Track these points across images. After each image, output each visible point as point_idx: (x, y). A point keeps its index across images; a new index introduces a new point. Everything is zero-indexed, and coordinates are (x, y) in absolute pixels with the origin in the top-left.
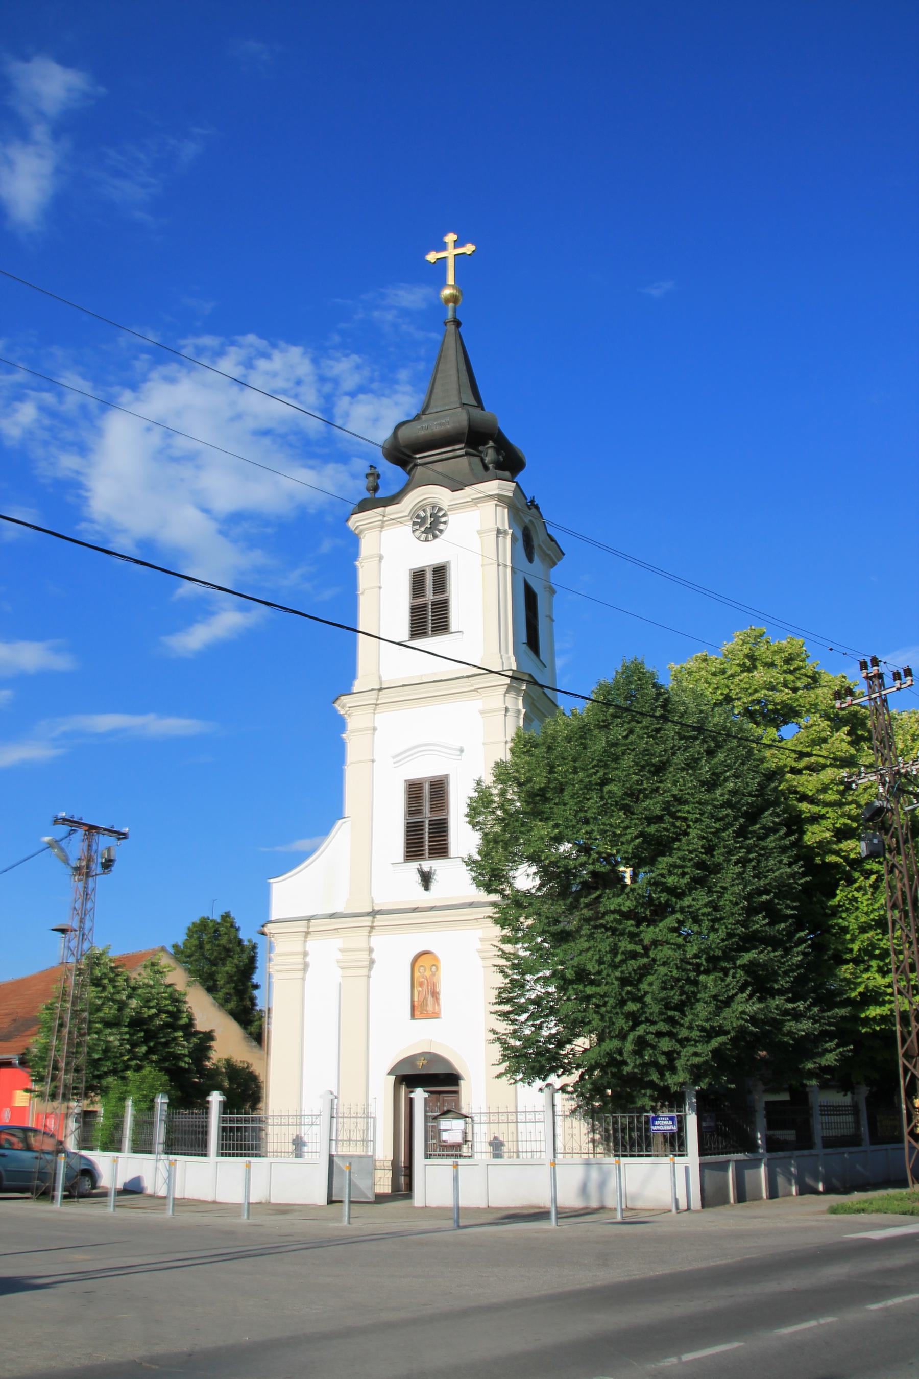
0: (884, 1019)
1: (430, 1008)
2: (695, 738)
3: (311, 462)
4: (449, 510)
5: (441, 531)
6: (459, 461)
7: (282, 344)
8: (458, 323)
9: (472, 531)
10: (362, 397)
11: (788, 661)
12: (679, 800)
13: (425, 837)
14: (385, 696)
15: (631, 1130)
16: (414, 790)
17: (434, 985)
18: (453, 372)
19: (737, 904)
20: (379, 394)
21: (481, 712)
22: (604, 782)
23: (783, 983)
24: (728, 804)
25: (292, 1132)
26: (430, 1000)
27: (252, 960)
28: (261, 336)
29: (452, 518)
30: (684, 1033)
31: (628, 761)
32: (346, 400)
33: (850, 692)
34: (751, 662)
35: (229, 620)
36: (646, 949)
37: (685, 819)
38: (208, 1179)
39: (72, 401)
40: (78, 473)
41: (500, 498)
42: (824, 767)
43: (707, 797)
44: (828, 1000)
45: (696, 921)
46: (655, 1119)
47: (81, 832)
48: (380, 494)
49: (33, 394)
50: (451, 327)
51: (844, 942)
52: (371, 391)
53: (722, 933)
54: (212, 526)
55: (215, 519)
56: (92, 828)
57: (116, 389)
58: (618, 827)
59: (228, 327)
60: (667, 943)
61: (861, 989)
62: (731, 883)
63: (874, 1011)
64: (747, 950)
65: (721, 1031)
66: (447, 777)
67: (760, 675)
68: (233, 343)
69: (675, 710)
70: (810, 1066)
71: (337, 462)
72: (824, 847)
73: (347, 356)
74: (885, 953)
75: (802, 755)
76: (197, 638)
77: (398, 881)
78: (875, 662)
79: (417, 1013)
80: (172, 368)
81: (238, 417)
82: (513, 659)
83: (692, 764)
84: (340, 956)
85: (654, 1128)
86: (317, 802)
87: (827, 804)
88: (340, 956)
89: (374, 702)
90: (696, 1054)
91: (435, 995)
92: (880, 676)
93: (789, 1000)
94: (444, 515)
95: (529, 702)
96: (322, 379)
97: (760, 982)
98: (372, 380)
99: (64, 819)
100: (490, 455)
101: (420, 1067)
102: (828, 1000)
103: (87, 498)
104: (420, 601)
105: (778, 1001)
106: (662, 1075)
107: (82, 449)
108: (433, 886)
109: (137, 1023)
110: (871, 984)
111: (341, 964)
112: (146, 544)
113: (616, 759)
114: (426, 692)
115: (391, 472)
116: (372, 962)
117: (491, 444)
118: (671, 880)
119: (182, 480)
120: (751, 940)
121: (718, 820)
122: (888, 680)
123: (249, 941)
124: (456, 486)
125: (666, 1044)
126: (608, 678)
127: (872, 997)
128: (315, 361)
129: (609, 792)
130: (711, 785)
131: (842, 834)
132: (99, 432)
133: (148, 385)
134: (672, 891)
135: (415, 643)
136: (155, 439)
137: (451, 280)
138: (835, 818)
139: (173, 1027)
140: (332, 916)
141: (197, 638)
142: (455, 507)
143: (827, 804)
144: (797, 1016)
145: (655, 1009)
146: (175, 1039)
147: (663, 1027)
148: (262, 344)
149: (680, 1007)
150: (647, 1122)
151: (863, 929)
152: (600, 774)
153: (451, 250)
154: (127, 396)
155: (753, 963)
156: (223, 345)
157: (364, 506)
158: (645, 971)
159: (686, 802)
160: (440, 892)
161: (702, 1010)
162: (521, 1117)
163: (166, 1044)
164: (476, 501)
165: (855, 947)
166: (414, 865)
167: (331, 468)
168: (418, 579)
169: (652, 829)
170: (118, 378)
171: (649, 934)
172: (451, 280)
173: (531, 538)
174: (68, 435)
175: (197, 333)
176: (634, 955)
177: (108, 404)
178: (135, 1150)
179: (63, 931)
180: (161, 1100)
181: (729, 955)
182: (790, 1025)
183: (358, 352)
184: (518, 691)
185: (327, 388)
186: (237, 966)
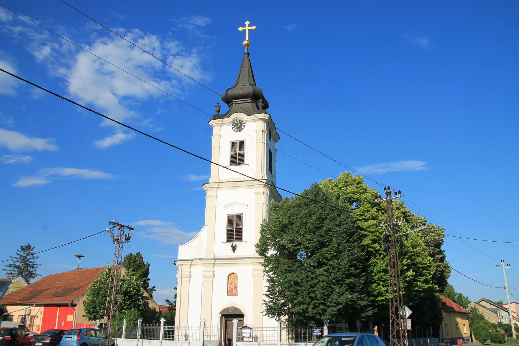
0: (382, 301)
1: (234, 292)
2: (335, 210)
3: (156, 79)
5: (243, 129)
6: (249, 104)
7: (149, 34)
8: (248, 54)
9: (253, 131)
10: (177, 57)
11: (358, 184)
12: (330, 231)
13: (234, 233)
15: (306, 334)
16: (230, 218)
18: (247, 72)
19: (346, 264)
20: (184, 56)
21: (255, 193)
22: (306, 223)
23: (357, 289)
24: (344, 232)
25: (185, 332)
27: (148, 270)
28: (141, 30)
29: (246, 125)
30: (329, 304)
31: (314, 217)
32: (172, 57)
33: (380, 197)
34: (347, 184)
35: (120, 137)
36: (317, 277)
37: (331, 236)
39: (65, 48)
40: (65, 75)
41: (264, 120)
42: (369, 220)
43: (339, 229)
44: (369, 294)
45: (333, 269)
47: (118, 227)
48: (219, 114)
49: (50, 43)
50: (246, 55)
51: (372, 276)
52: (182, 55)
53: (341, 272)
54: (116, 100)
55: (118, 97)
56: (122, 226)
57: (83, 45)
58: (311, 238)
59: (129, 26)
60: (323, 275)
61: (377, 292)
62: (345, 257)
63: (380, 298)
64: (348, 279)
65: (339, 304)
67: (350, 189)
68: (130, 32)
69: (329, 201)
70: (363, 315)
71: (166, 80)
72: (368, 246)
73: (173, 41)
74: (386, 280)
75: (361, 215)
76: (107, 142)
77: (224, 248)
78: (389, 188)
79: (229, 293)
80: (106, 39)
81: (130, 60)
82: (266, 175)
83: (334, 219)
84: (202, 273)
86: (193, 220)
87: (370, 232)
88: (202, 273)
90: (333, 311)
91: (236, 288)
92: (390, 193)
93: (359, 294)
94: (244, 123)
95: (270, 191)
96: (163, 49)
97: (351, 288)
98: (182, 51)
99: (113, 223)
100: (260, 104)
101: (231, 312)
102: (369, 294)
103: (67, 86)
104: (234, 153)
105: (356, 295)
106: (321, 316)
107: (68, 67)
108: (236, 251)
109: (126, 293)
110: (381, 290)
112: (91, 104)
113: (310, 216)
115: (224, 107)
116: (214, 276)
117: (261, 100)
118: (326, 255)
119: (106, 82)
120: (349, 276)
121: (342, 237)
122: (393, 194)
123: (147, 263)
124: (249, 114)
125: (322, 307)
126: (308, 188)
127: (380, 294)
128: (161, 42)
129: (308, 227)
130: (339, 225)
131: (374, 241)
132: (75, 61)
133: (95, 44)
134: (326, 258)
135: (234, 168)
136: (97, 65)
137: (247, 39)
138: (372, 236)
139: (138, 295)
140: (200, 259)
141: (107, 142)
142: (248, 121)
143: (370, 232)
144: (361, 299)
145: (319, 296)
146: (139, 299)
147: (322, 301)
148: (141, 33)
149: (328, 295)
150: (312, 331)
151: (379, 272)
152: (305, 220)
153: (247, 27)
154: (87, 48)
155: (350, 283)
156: (125, 32)
157: (216, 117)
158: (316, 284)
159: (332, 231)
160: (239, 252)
161: (335, 297)
163: (135, 301)
164: (255, 120)
165: (376, 277)
166: (231, 243)
167: (163, 83)
168: (234, 145)
169: (321, 239)
170: (84, 41)
171: (318, 272)
172: (247, 39)
173: (272, 133)
174: (63, 61)
175: (117, 27)
176: (312, 279)
177: (80, 49)
178: (127, 337)
179: (79, 257)
180: (140, 321)
181: (343, 279)
182: (359, 302)
183: (178, 40)
184: (267, 187)
185: (165, 52)
186: (143, 272)
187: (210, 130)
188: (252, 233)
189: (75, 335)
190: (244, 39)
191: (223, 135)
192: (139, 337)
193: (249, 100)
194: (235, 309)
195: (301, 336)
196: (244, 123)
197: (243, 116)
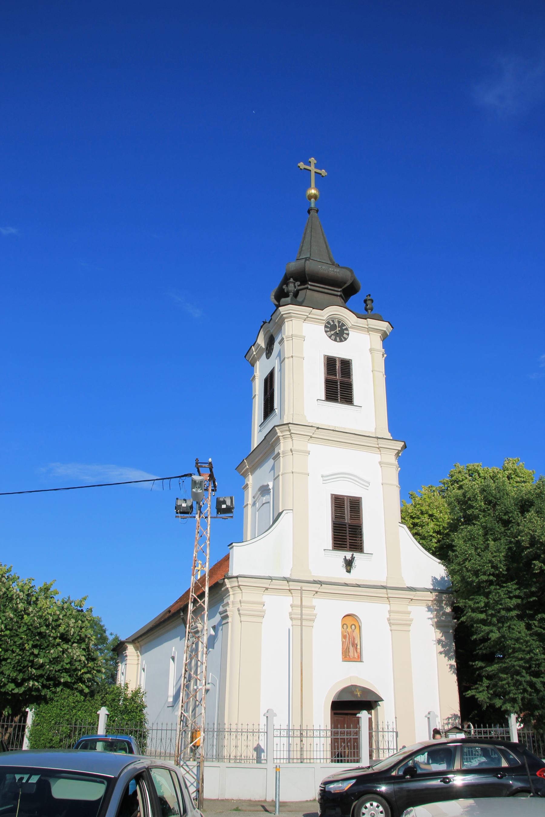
1: (351, 654)
4: (351, 328)
5: (346, 339)
9: (365, 347)
13: (347, 531)
14: (320, 434)
16: (338, 502)
17: (354, 638)
26: (351, 649)
29: (351, 333)
66: (332, 495)
89: (311, 434)
91: (354, 645)
142: (355, 327)
164: (369, 330)
188: (381, 519)
193: (338, 291)
194: (366, 691)
196: (347, 329)
197: (348, 317)
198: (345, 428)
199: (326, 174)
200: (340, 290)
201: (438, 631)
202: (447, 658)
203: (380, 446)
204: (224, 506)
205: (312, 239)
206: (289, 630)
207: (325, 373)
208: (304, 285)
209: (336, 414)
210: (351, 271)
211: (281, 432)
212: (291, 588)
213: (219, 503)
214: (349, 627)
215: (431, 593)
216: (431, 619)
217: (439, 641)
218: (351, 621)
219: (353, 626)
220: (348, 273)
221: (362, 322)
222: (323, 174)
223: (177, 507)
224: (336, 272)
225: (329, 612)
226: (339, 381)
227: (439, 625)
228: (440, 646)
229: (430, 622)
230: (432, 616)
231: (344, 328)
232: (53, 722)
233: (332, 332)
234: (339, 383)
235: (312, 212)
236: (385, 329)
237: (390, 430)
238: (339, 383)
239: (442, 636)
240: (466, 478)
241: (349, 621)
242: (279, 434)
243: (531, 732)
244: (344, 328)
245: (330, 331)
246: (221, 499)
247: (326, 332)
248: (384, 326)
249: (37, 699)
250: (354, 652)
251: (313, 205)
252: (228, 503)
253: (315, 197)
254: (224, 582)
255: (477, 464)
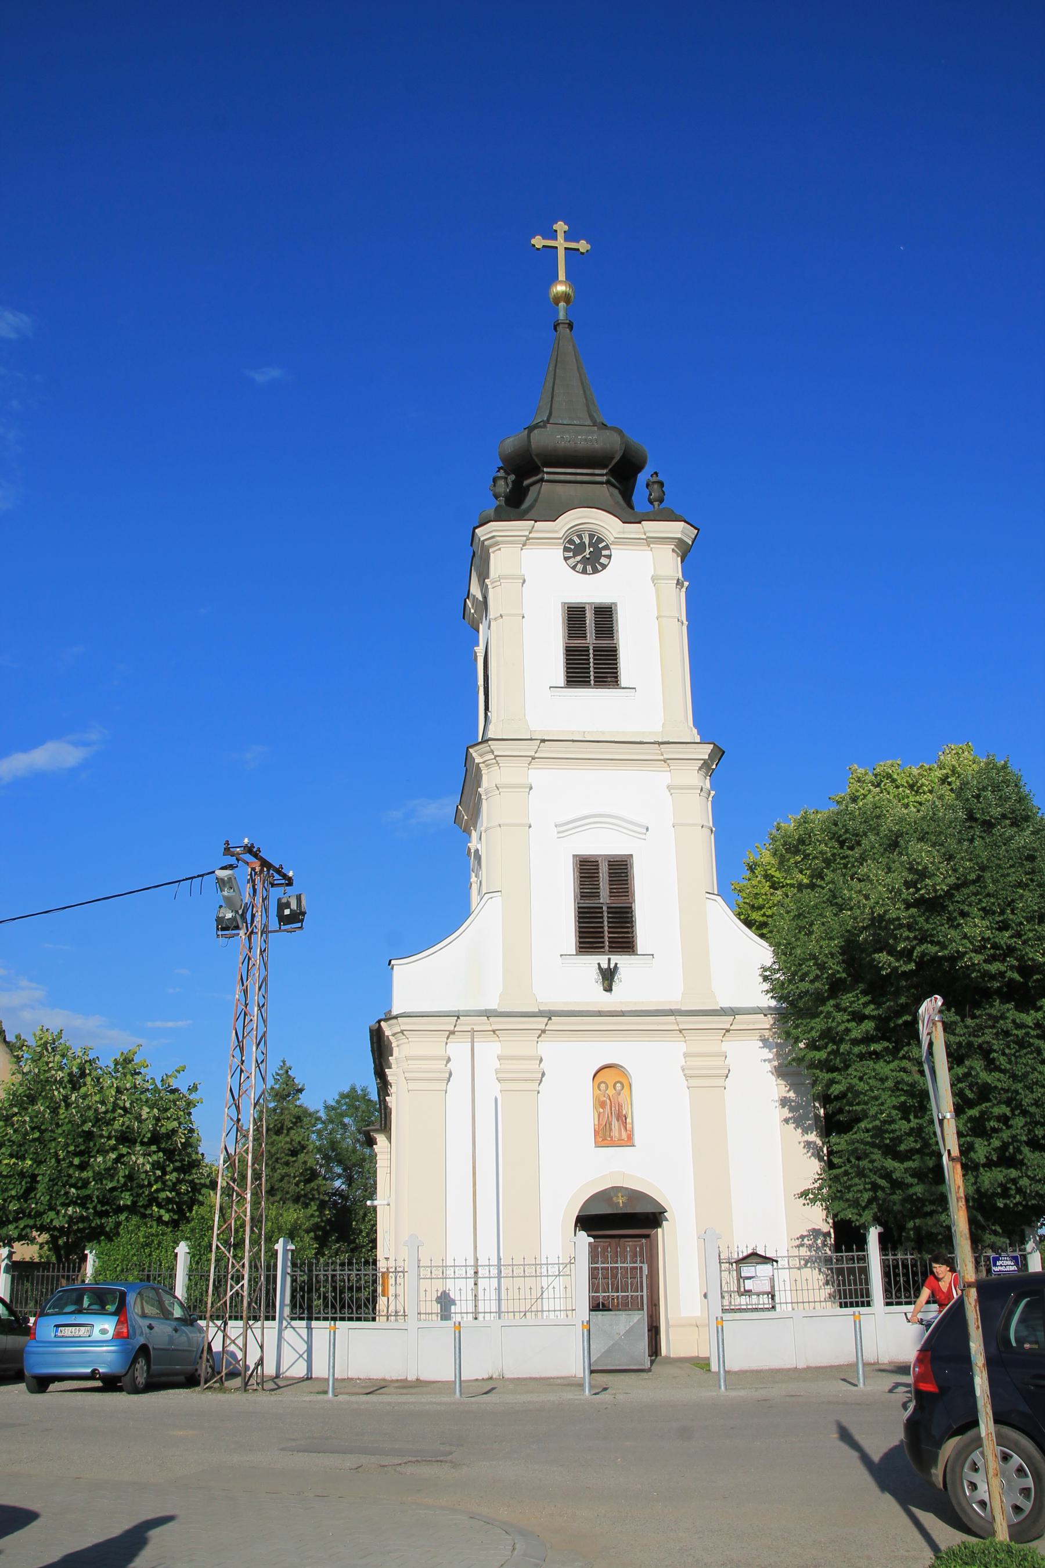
1: (615, 1133)
4: (613, 543)
5: (604, 567)
9: (643, 577)
13: (605, 917)
14: (546, 750)
16: (587, 869)
17: (620, 1106)
25: (438, 1286)
29: (616, 552)
38: (351, 1350)
41: (680, 542)
46: (996, 1260)
66: (574, 856)
85: (996, 1269)
91: (622, 1118)
94: (607, 547)
104: (577, 643)
111: (499, 1075)
114: (552, 752)
123: (18, 1037)
137: (562, 276)
142: (621, 541)
160: (624, 994)
162: (450, 1272)
164: (650, 541)
187: (478, 560)
189: (102, 1312)
190: (555, 278)
191: (524, 580)
192: (287, 1310)
193: (601, 474)
194: (635, 1196)
195: (897, 1282)
196: (607, 547)
197: (607, 524)
198: (603, 733)
199: (589, 247)
200: (605, 471)
201: (782, 1082)
202: (799, 1130)
203: (666, 756)
204: (287, 912)
205: (557, 381)
206: (496, 1099)
207: (564, 637)
208: (536, 475)
209: (592, 709)
210: (620, 432)
211: (481, 755)
212: (494, 1027)
213: (282, 906)
214: (611, 1086)
215: (765, 1015)
216: (770, 1061)
217: (784, 1102)
218: (610, 1076)
219: (618, 1085)
220: (616, 438)
221: (633, 530)
222: (582, 250)
223: (219, 920)
224: (591, 441)
225: (570, 1064)
226: (591, 648)
227: (781, 1072)
228: (786, 1110)
229: (768, 1067)
230: (771, 1056)
231: (600, 546)
232: (118, 1269)
233: (579, 558)
234: (591, 651)
235: (560, 328)
236: (679, 536)
237: (696, 724)
238: (591, 651)
239: (789, 1091)
240: (870, 791)
241: (608, 1076)
242: (476, 761)
243: (909, 1257)
244: (600, 546)
245: (574, 556)
246: (284, 901)
247: (566, 559)
248: (677, 529)
249: (96, 1234)
250: (620, 1130)
251: (562, 315)
252: (294, 906)
253: (566, 298)
254: (380, 1026)
255: (889, 762)
